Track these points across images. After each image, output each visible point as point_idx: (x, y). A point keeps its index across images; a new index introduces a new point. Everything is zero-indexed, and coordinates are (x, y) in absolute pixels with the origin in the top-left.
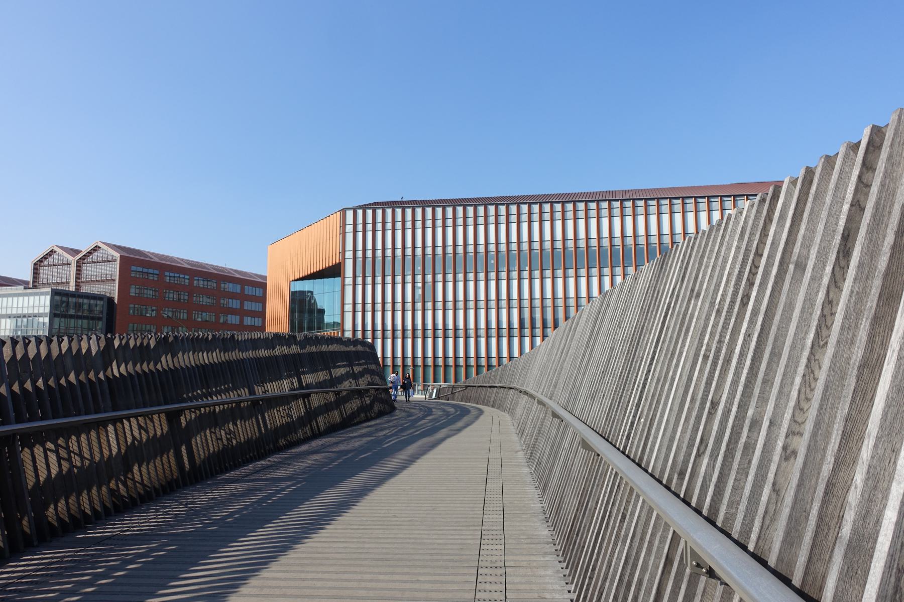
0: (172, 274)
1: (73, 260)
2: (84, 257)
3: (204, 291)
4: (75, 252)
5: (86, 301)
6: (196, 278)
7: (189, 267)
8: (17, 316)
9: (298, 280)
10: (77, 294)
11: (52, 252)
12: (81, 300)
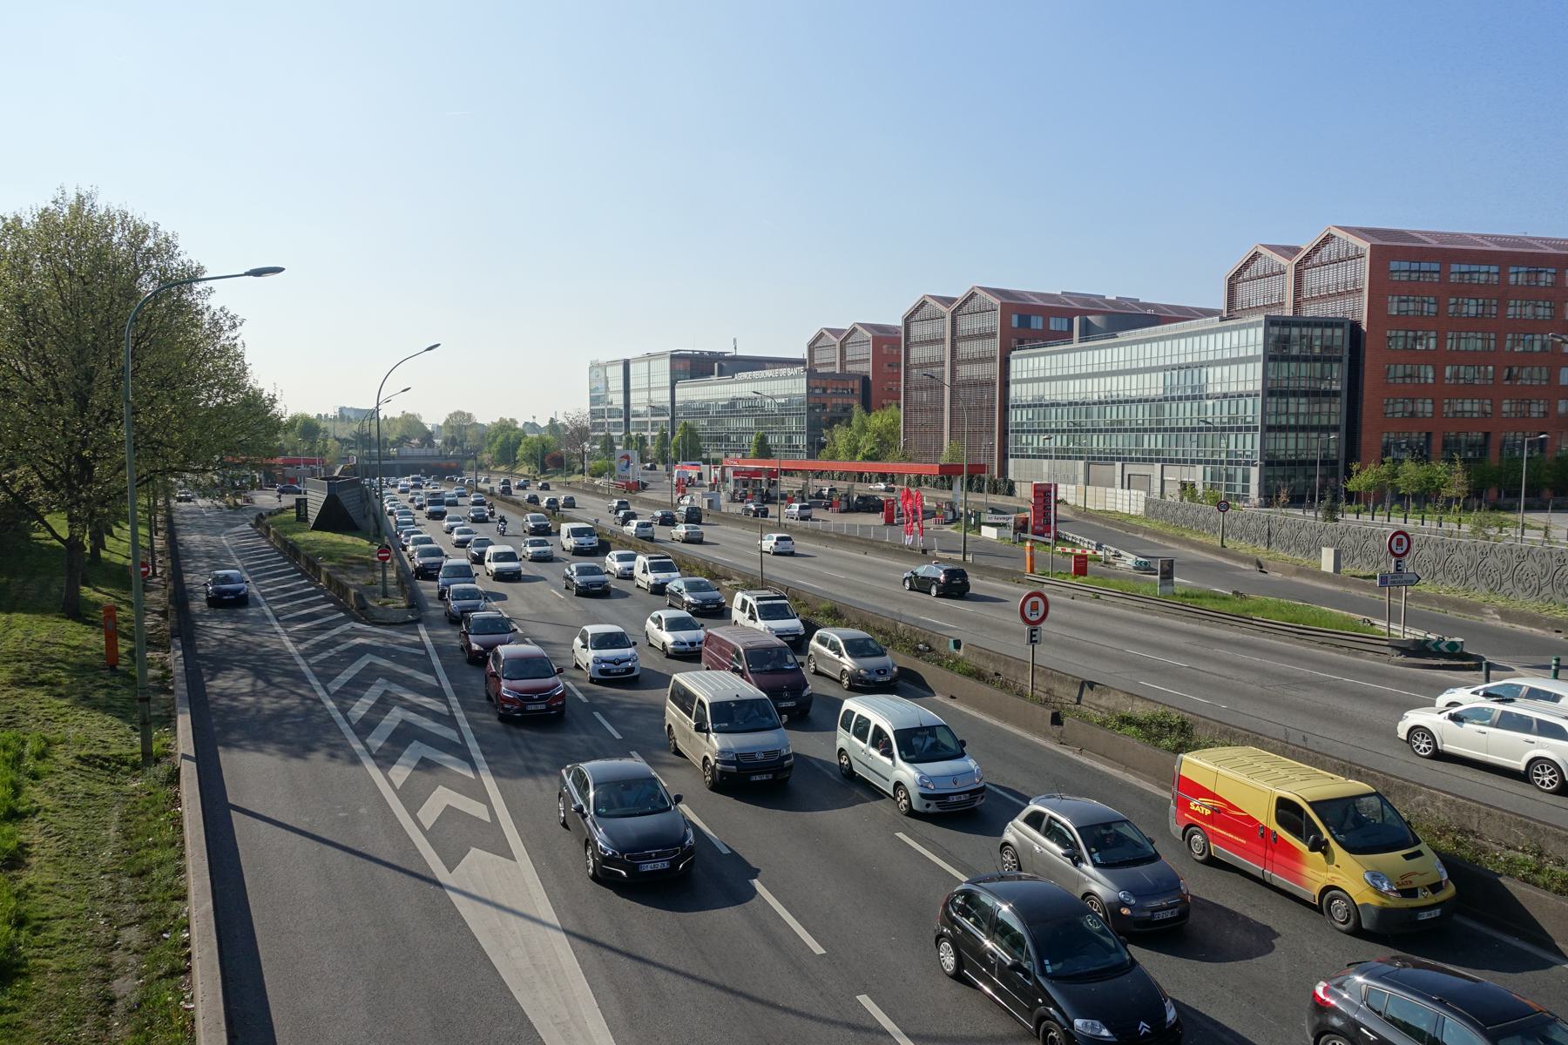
0: (1464, 268)
1: (1289, 265)
2: (1308, 257)
3: (1530, 294)
4: (1291, 251)
5: (1318, 332)
6: (1512, 269)
7: (1555, 251)
8: (1165, 369)
9: (247, 274)
10: (1297, 322)
11: (1255, 257)
12: (1286, 331)
